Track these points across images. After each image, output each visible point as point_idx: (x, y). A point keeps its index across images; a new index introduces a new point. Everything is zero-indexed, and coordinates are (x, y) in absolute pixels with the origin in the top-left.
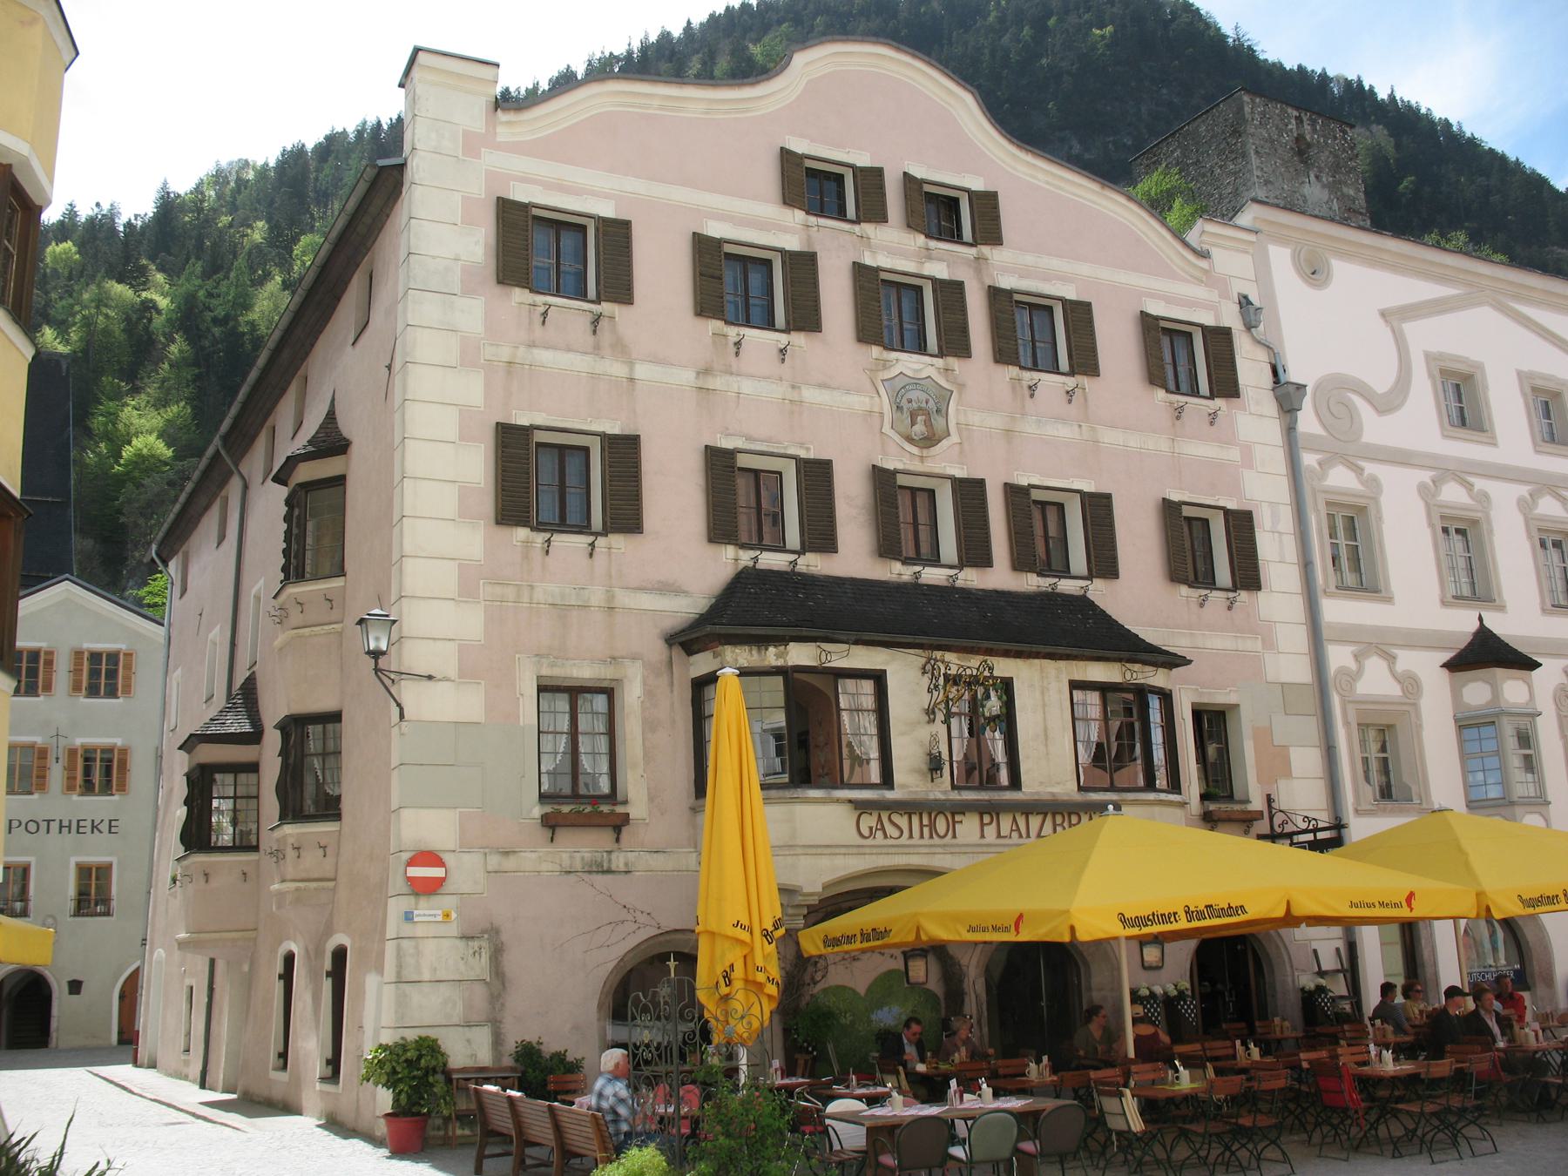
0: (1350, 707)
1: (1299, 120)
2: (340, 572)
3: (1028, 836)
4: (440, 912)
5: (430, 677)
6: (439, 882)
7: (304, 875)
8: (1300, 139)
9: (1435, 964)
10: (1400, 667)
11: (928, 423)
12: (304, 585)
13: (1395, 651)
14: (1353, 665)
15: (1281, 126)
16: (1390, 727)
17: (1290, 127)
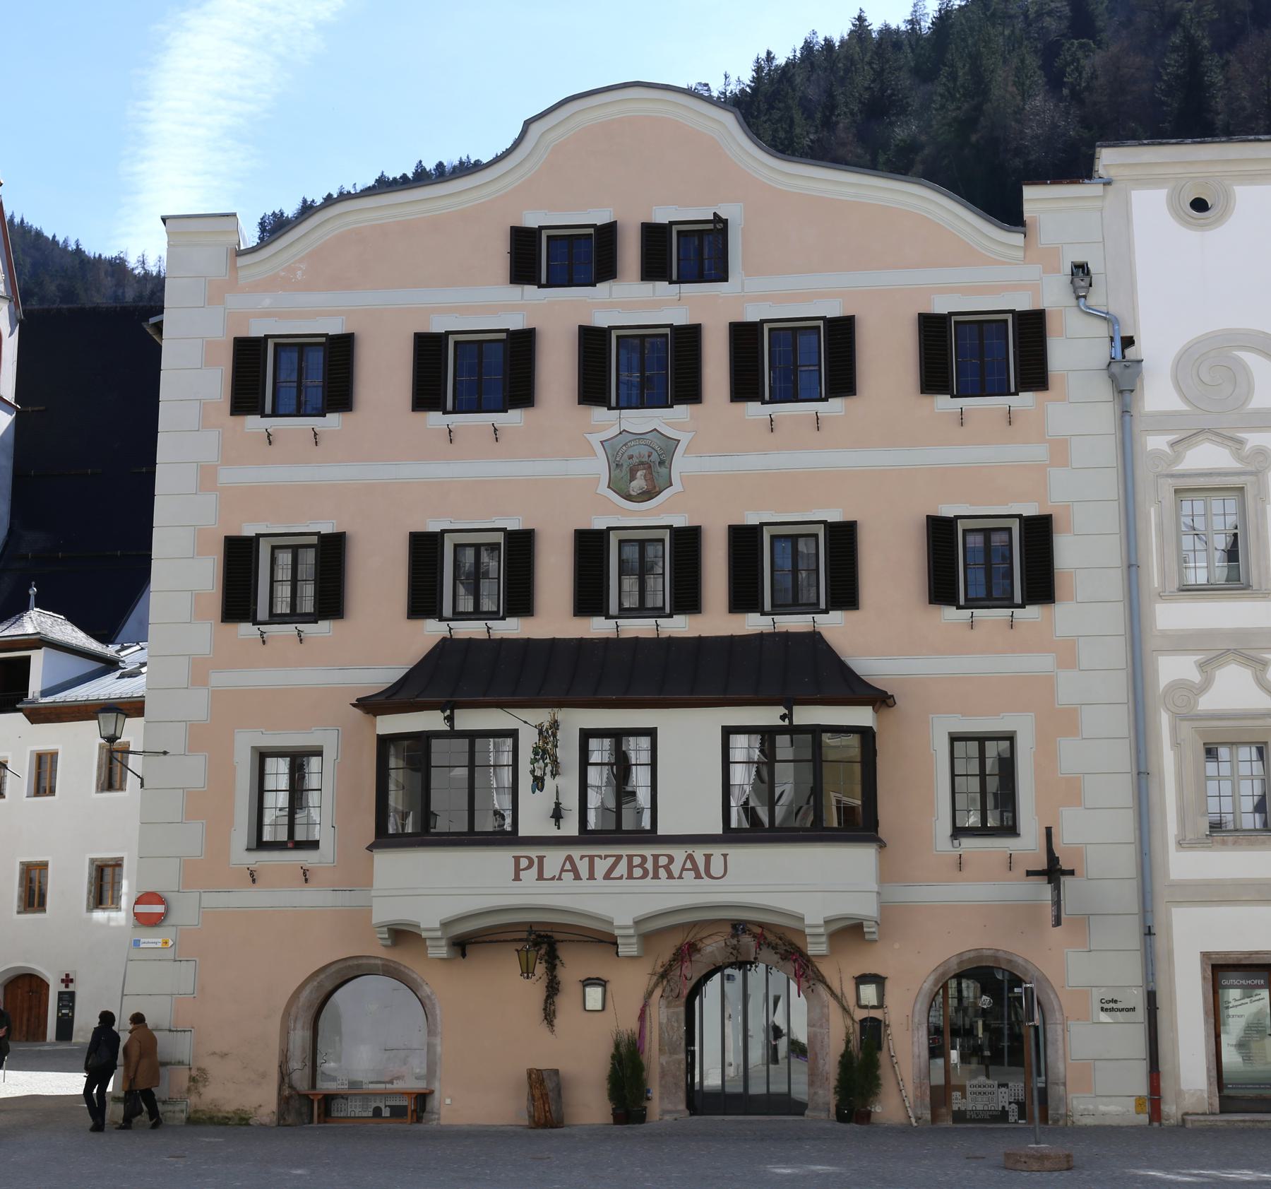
3: (592, 877)
4: (160, 940)
5: (165, 753)
11: (650, 478)
14: (1195, 676)
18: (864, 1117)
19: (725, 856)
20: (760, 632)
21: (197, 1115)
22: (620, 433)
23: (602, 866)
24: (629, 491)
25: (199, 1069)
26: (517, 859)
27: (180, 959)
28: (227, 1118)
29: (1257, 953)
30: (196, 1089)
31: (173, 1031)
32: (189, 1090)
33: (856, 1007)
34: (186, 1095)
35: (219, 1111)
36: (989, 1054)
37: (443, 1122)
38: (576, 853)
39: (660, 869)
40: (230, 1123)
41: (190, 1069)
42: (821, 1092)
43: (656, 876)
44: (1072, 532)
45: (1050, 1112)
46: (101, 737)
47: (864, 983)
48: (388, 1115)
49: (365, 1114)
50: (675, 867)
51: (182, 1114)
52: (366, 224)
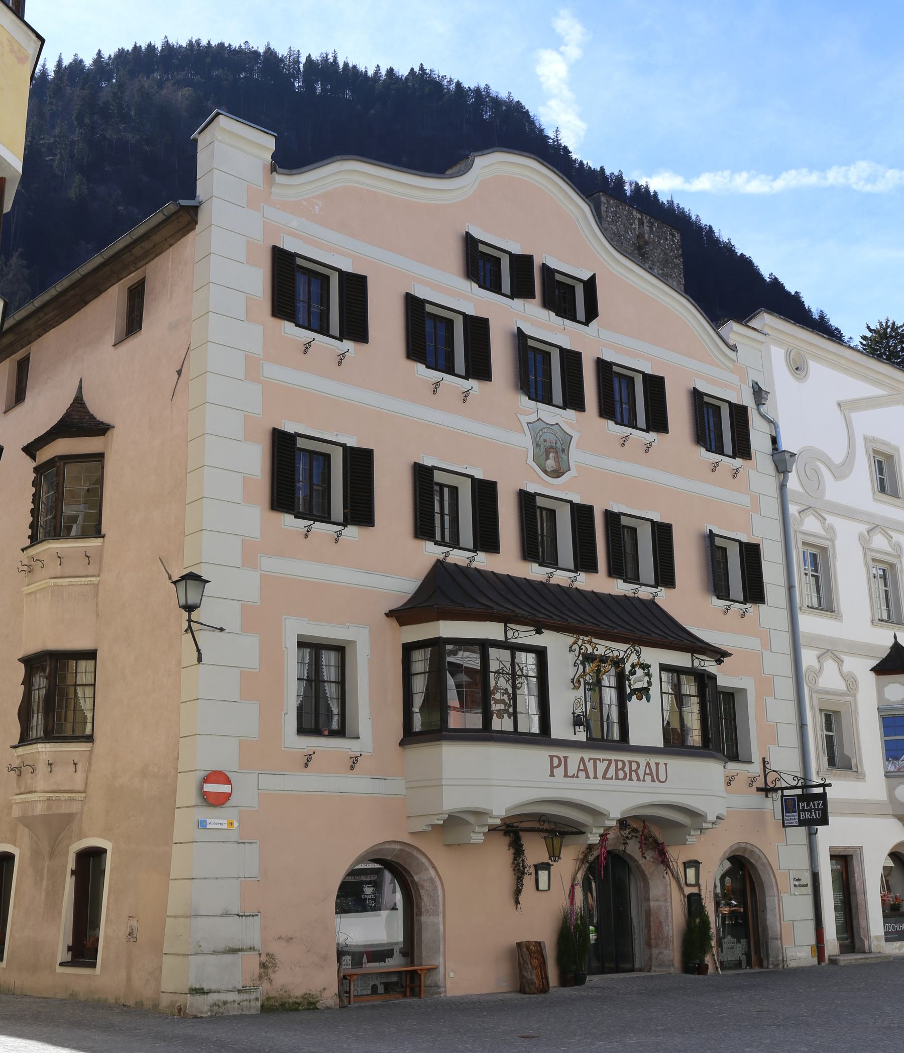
0: (814, 695)
1: (641, 223)
2: (96, 532)
5: (221, 630)
6: (228, 796)
7: (55, 788)
8: (640, 236)
9: (864, 893)
10: (846, 668)
11: (557, 460)
12: (62, 543)
13: (843, 657)
15: (627, 224)
16: (837, 713)
17: (634, 226)
18: (702, 969)
19: (666, 764)
20: (623, 594)
21: (270, 1003)
22: (538, 420)
23: (601, 766)
24: (545, 467)
25: (268, 955)
26: (551, 757)
27: (243, 841)
28: (296, 1003)
29: (849, 847)
30: (267, 975)
31: (242, 916)
32: (260, 977)
33: (685, 886)
34: (258, 983)
35: (289, 996)
36: (590, 927)
37: (449, 994)
38: (587, 755)
39: (619, 771)
40: (300, 1008)
41: (260, 954)
42: (666, 952)
43: (631, 779)
44: (259, 568)
45: (771, 959)
46: (180, 607)
47: (689, 867)
48: (383, 992)
49: (365, 992)
50: (641, 772)
51: (257, 1003)
52: (364, 187)
